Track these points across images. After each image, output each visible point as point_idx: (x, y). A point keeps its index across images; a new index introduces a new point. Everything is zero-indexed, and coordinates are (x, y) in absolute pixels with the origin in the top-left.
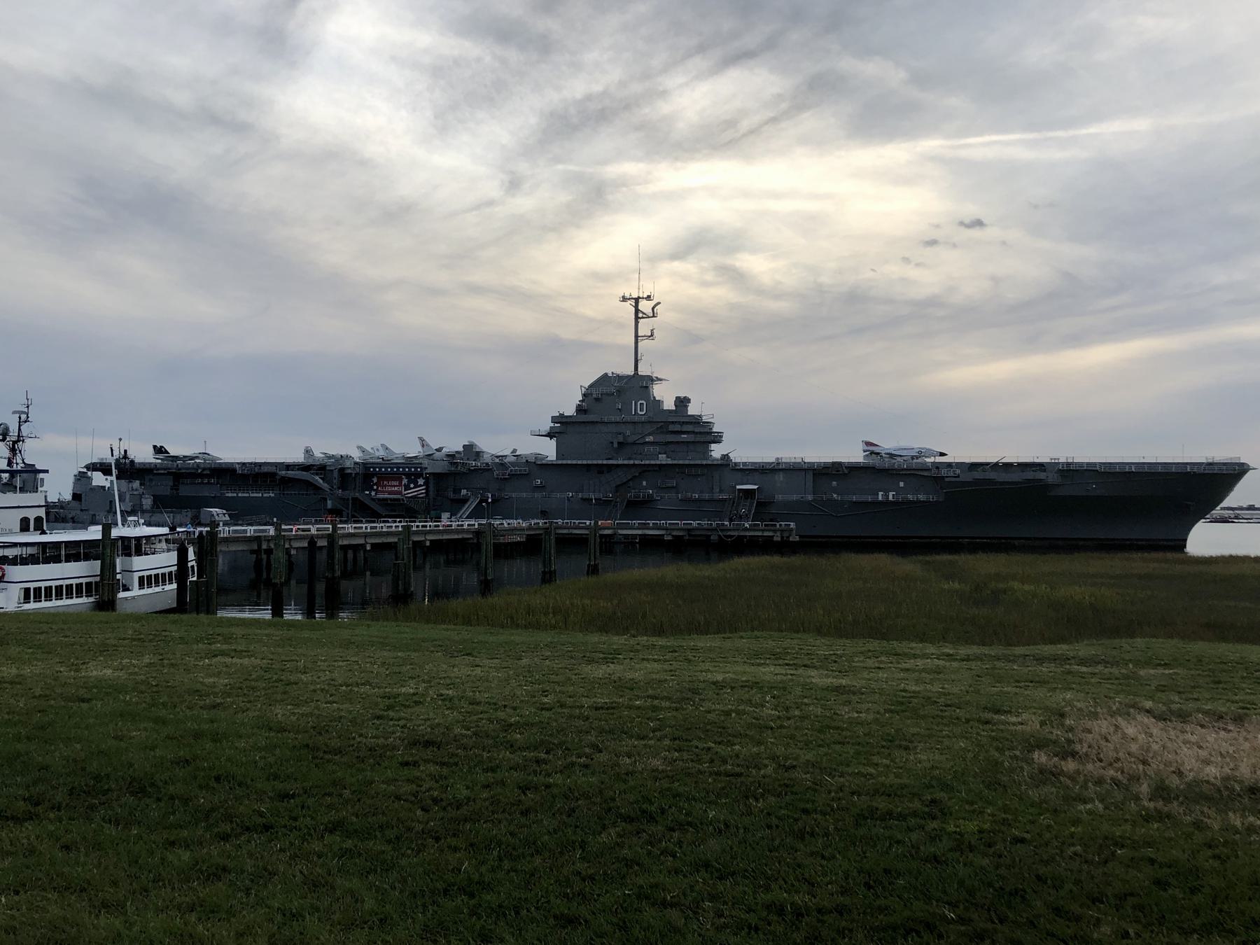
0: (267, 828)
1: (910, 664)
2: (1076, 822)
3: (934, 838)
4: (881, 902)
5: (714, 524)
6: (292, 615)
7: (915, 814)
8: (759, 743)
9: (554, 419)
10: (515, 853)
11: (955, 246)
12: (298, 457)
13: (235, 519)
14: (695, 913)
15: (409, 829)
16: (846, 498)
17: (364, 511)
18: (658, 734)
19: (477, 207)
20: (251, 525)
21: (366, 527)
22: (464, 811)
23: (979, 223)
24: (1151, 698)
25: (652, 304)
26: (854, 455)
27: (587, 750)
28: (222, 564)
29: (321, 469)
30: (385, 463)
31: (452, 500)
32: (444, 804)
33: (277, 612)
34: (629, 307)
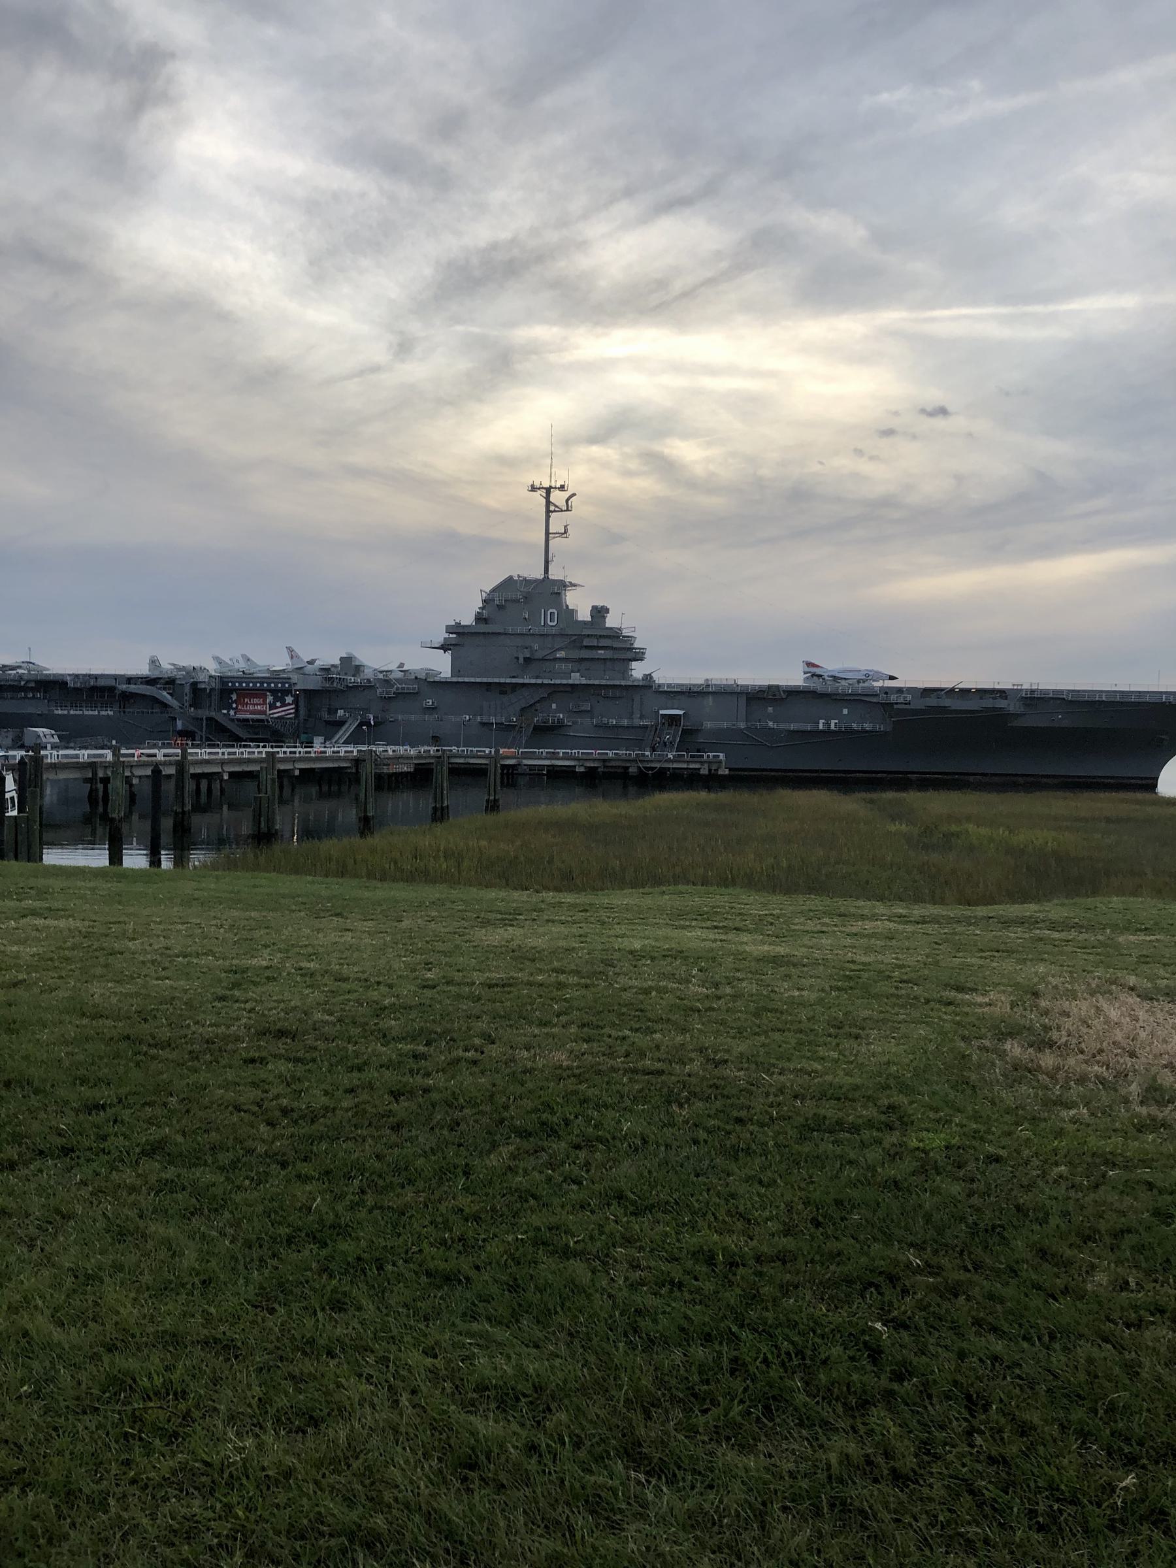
0: (66, 1151)
1: (857, 927)
2: (1060, 1133)
3: (893, 1156)
4: (833, 1246)
5: (633, 755)
6: (135, 859)
7: (870, 1124)
8: (684, 1030)
9: (449, 629)
10: (381, 1182)
11: (914, 437)
12: (143, 670)
13: (66, 741)
14: (604, 1263)
15: (250, 1151)
16: (783, 726)
17: (220, 733)
18: (563, 1019)
19: (361, 373)
20: (86, 748)
21: (223, 752)
22: (319, 1127)
23: (942, 411)
24: (1134, 971)
25: (566, 495)
26: (794, 677)
27: (477, 1041)
28: (50, 794)
29: (170, 683)
30: (246, 677)
31: (328, 723)
32: (295, 1115)
33: (116, 858)
34: (539, 498)
